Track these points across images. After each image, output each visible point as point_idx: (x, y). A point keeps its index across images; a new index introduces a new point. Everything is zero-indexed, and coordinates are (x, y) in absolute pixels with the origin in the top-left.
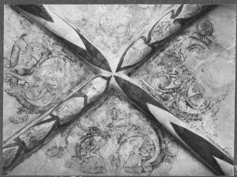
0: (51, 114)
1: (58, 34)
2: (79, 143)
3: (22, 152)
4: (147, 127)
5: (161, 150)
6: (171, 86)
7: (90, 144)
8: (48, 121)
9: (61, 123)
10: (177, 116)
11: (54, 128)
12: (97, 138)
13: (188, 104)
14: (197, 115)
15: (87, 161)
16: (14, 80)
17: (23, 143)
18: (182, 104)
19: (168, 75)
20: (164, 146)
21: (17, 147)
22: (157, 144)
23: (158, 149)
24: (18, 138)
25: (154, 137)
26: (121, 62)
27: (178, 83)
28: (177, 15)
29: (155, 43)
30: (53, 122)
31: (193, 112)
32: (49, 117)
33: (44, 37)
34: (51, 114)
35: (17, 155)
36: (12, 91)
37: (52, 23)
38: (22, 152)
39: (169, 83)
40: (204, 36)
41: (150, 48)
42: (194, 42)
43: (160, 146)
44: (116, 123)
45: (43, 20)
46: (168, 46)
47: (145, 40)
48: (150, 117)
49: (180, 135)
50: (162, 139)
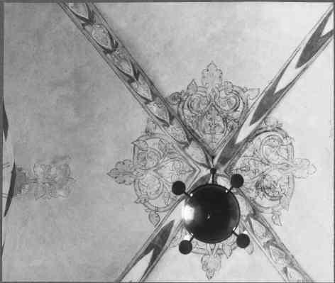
0: (245, 221)
1: (161, 92)
2: (269, 198)
3: (275, 243)
4: (256, 142)
5: (273, 130)
6: (221, 123)
7: (270, 188)
8: (250, 223)
9: (252, 212)
10: (245, 119)
11: (255, 219)
12: (266, 183)
13: (235, 110)
14: (244, 103)
15: (283, 191)
16: (219, 252)
17: (268, 242)
18: (236, 115)
19: (213, 126)
20: (269, 128)
21: (270, 247)
22: (269, 134)
23: (272, 133)
24: (264, 247)
25: (263, 136)
26: (203, 165)
27: (219, 118)
28: (167, 123)
29: (188, 138)
30: (252, 220)
31: (241, 106)
32: (248, 223)
33: (174, 164)
34: (245, 221)
35: (276, 246)
36: (228, 254)
37: (295, 66)
38: (275, 243)
39: (218, 125)
40: (181, 99)
41: (192, 142)
42: (186, 106)
43: (269, 131)
44: (253, 168)
45: (173, 229)
46: (189, 127)
47: (186, 146)
48: (249, 139)
49: (259, 118)
50: (264, 130)
